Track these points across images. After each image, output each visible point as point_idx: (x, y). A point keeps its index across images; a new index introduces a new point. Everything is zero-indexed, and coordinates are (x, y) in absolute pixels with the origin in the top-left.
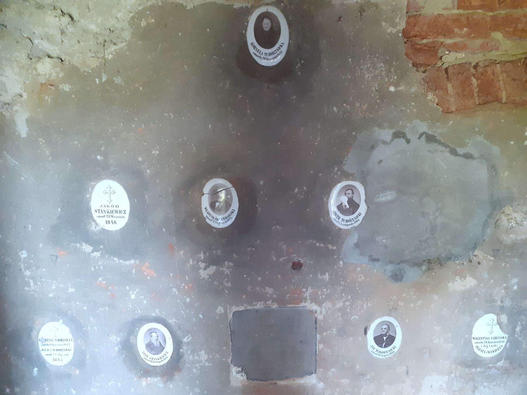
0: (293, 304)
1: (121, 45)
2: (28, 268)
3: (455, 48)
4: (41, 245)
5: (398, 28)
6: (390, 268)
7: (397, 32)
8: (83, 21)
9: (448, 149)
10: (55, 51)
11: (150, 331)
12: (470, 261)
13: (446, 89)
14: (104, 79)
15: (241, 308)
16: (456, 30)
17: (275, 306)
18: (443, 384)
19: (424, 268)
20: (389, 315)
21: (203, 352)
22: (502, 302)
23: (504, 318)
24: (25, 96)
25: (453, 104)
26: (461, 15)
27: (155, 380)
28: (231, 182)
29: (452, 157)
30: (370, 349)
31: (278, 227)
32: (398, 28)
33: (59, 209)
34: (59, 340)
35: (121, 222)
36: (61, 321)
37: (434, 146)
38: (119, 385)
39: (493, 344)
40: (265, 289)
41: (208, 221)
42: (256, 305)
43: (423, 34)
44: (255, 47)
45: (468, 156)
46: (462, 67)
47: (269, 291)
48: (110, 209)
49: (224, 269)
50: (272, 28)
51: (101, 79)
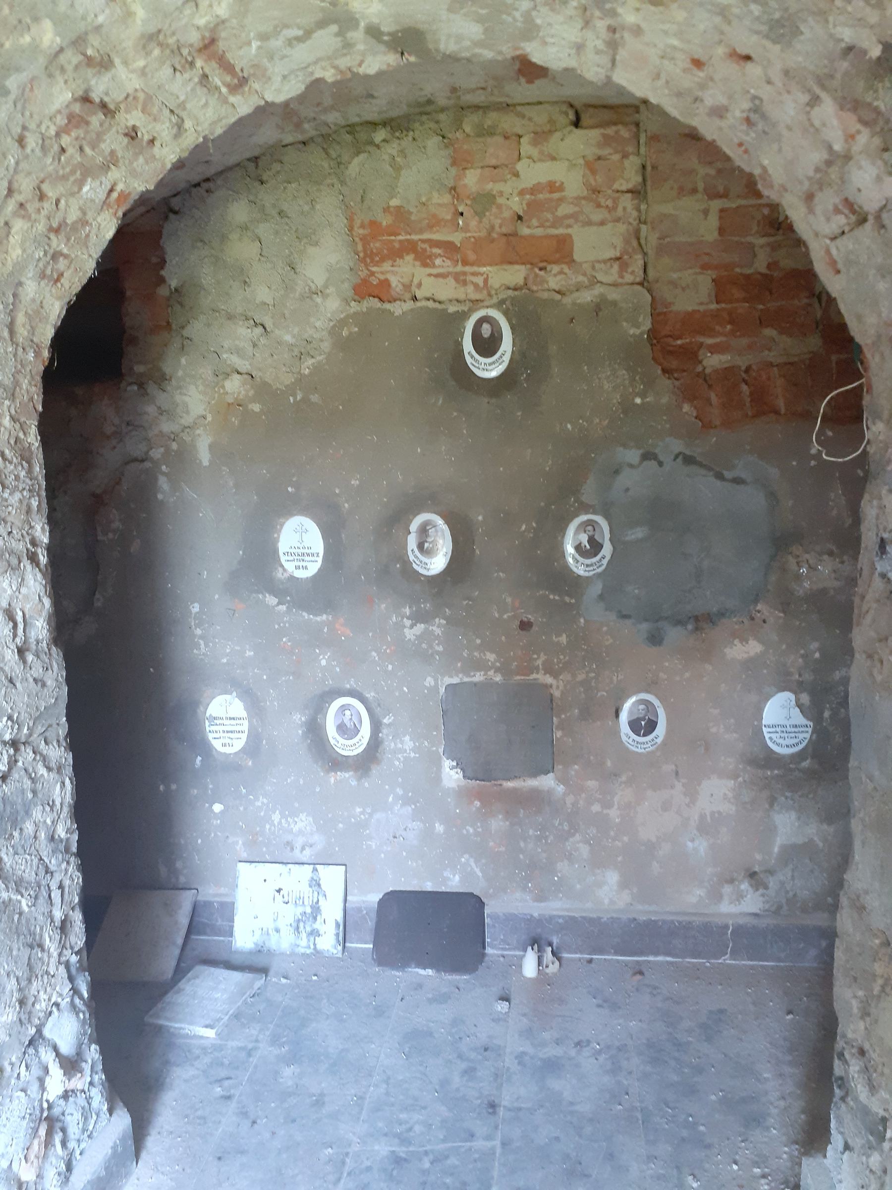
3: (714, 349)
4: (217, 597)
6: (645, 626)
7: (642, 334)
8: (277, 332)
10: (243, 365)
11: (344, 708)
12: (752, 619)
14: (299, 398)
15: (455, 680)
17: (498, 678)
18: (727, 792)
19: (690, 627)
21: (407, 738)
22: (800, 675)
23: (805, 698)
24: (209, 418)
26: (723, 309)
27: (347, 775)
29: (718, 483)
30: (624, 738)
31: (501, 574)
33: (241, 552)
34: (230, 719)
35: (313, 568)
36: (234, 694)
37: (694, 469)
40: (485, 655)
41: (414, 566)
42: (474, 676)
44: (472, 357)
45: (738, 481)
46: (729, 372)
48: (301, 551)
49: (434, 628)
50: (492, 334)
51: (295, 398)
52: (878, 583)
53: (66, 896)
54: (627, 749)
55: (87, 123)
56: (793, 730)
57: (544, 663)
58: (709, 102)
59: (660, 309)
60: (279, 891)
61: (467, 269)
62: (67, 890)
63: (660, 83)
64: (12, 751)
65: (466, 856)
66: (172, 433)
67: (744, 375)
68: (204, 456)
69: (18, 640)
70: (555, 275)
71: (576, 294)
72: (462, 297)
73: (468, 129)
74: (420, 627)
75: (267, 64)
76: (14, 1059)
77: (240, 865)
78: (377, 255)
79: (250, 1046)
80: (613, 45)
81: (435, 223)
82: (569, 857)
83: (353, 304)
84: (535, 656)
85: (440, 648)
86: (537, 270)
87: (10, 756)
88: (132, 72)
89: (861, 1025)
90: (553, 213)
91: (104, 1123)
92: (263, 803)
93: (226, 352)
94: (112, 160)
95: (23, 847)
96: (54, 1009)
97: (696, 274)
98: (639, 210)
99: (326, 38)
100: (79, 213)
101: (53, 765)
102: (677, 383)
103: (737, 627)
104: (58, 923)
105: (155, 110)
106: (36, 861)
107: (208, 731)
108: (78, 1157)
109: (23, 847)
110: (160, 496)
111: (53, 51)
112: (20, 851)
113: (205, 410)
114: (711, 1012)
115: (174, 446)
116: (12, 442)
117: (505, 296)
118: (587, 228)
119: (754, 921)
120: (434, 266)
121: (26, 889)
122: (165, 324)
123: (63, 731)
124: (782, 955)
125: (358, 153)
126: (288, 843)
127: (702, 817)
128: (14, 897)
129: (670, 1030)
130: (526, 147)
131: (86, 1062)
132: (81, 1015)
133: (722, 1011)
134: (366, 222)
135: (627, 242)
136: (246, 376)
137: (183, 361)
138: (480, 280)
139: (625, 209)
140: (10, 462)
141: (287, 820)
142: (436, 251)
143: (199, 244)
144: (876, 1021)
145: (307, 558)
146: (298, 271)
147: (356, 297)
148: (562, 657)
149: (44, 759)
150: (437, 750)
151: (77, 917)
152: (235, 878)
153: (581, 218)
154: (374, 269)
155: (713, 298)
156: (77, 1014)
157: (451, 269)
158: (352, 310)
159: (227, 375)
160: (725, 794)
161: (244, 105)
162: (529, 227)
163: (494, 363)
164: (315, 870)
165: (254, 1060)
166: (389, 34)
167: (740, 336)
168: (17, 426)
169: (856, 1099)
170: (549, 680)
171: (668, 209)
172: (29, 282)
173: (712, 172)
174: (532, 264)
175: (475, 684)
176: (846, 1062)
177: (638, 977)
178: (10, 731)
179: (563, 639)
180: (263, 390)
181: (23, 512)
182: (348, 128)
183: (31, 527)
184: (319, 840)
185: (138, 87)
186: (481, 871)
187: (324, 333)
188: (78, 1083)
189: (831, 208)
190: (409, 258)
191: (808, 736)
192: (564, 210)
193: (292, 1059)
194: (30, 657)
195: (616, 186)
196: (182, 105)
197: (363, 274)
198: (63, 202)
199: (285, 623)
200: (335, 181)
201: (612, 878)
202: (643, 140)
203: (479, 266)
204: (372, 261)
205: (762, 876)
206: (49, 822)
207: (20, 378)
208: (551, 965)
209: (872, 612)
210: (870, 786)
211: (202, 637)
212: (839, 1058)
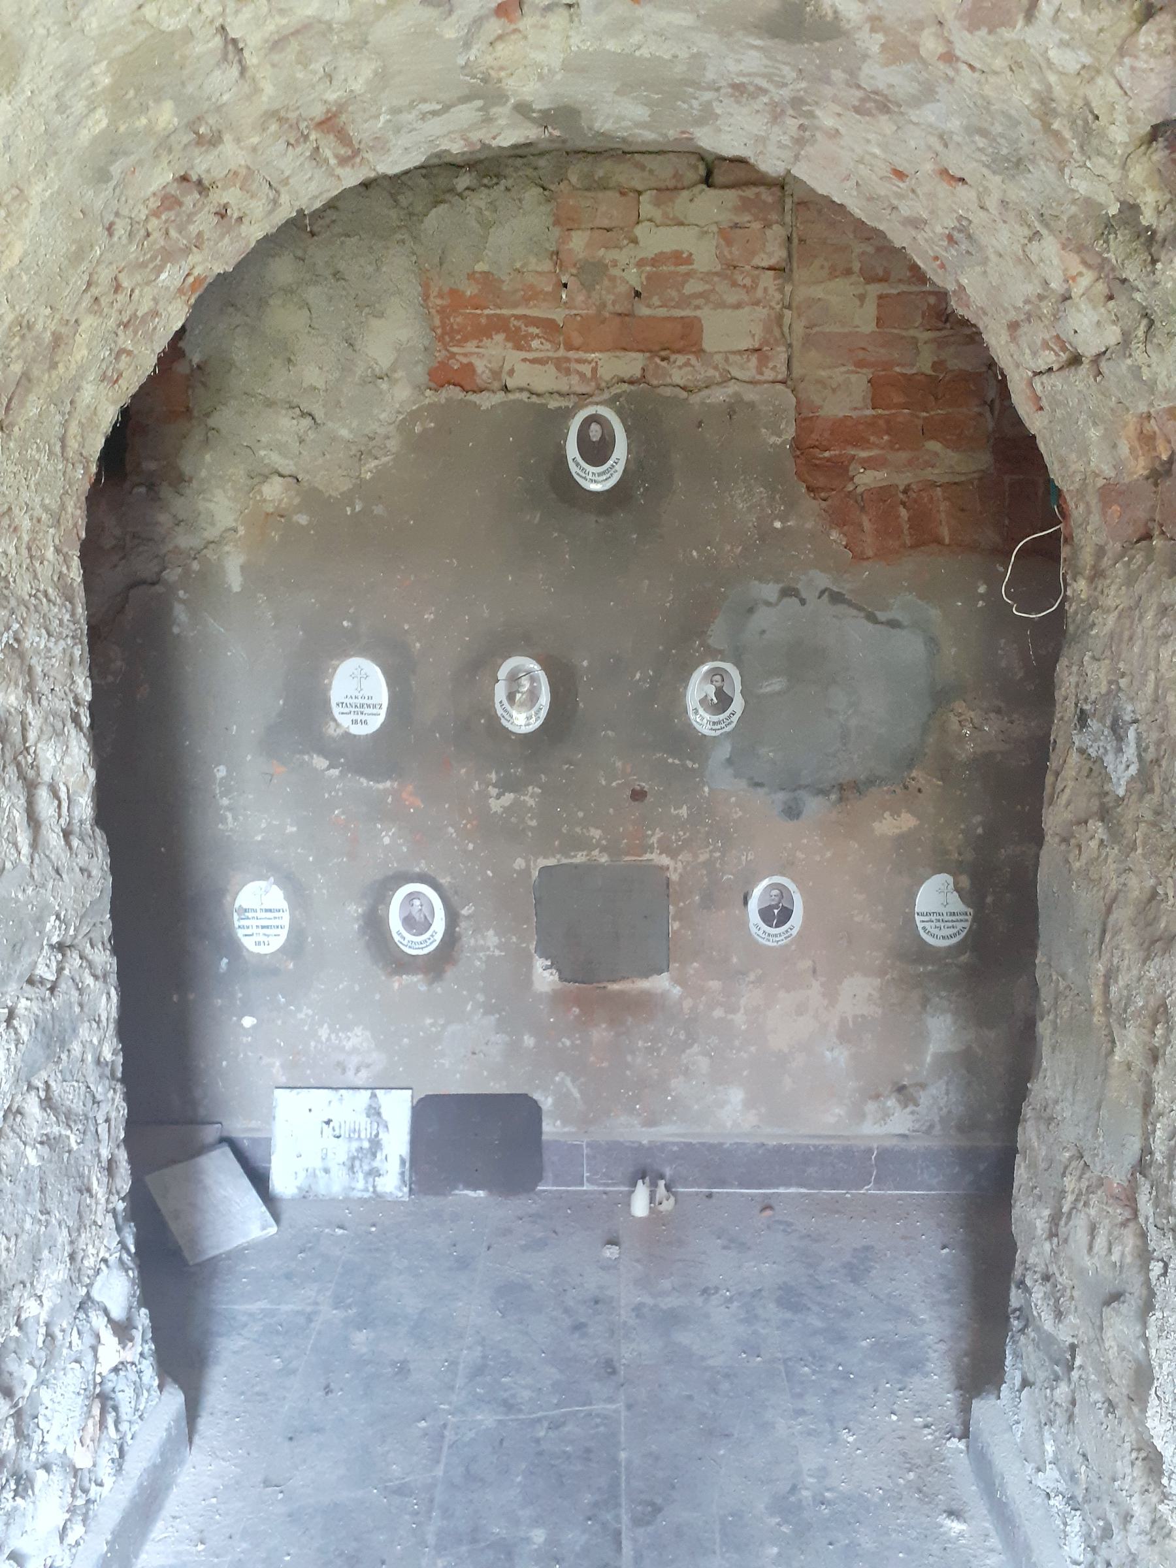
0: (633, 855)
1: (384, 459)
2: (224, 794)
3: (868, 464)
4: (249, 757)
5: (784, 437)
6: (781, 796)
7: (784, 443)
8: (330, 424)
9: (862, 614)
10: (286, 465)
11: (411, 896)
12: (906, 788)
13: (860, 525)
14: (358, 508)
15: (551, 862)
16: (872, 439)
17: (604, 859)
18: (873, 993)
19: (833, 797)
20: (783, 875)
21: (491, 933)
22: (960, 854)
23: (965, 881)
24: (242, 531)
25: (869, 543)
26: (879, 416)
27: (415, 979)
28: (539, 662)
29: (870, 626)
30: (753, 930)
31: (610, 733)
32: (784, 437)
33: (281, 702)
34: (266, 911)
35: (376, 721)
36: (272, 879)
37: (842, 608)
38: (357, 988)
39: (950, 924)
40: (588, 831)
41: (503, 721)
42: (575, 856)
43: (825, 443)
44: (578, 464)
45: (893, 624)
46: (883, 494)
47: (596, 833)
48: (361, 701)
49: (527, 798)
50: (603, 437)
51: (353, 509)
52: (1074, 758)
53: (112, 1131)
54: (757, 942)
55: (180, 204)
56: (951, 918)
57: (660, 840)
58: (905, 211)
59: (806, 413)
60: (328, 1122)
61: (572, 354)
62: (113, 1123)
63: (851, 183)
64: (60, 957)
65: (561, 1074)
66: (191, 548)
67: (901, 496)
68: (235, 580)
69: (62, 821)
70: (680, 368)
71: (705, 392)
72: (565, 389)
73: (574, 179)
74: (509, 798)
75: (391, 137)
76: (65, 1325)
77: (278, 1092)
78: (458, 332)
79: (309, 1309)
80: (800, 142)
81: (531, 295)
82: (686, 1072)
83: (428, 393)
84: (649, 832)
85: (534, 823)
86: (658, 360)
87: (59, 963)
88: (242, 149)
89: (1047, 1246)
90: (678, 291)
91: (154, 1403)
92: (306, 1015)
93: (264, 448)
94: (198, 242)
95: (71, 1072)
96: (103, 1266)
97: (848, 372)
98: (781, 290)
99: (466, 114)
100: (152, 303)
101: (99, 972)
102: (824, 504)
103: (887, 797)
104: (105, 1164)
105: (254, 187)
106: (83, 1088)
107: (236, 925)
108: (130, 1442)
109: (71, 1072)
110: (176, 630)
111: (166, 133)
112: (68, 1077)
113: (236, 520)
114: (855, 1250)
115: (195, 566)
116: (56, 579)
117: (619, 391)
118: (719, 310)
119: (903, 1144)
120: (530, 350)
121: (75, 1121)
122: (183, 409)
123: (106, 931)
124: (934, 1182)
125: (437, 203)
126: (339, 1064)
127: (843, 1021)
128: (63, 1132)
129: (811, 1272)
130: (647, 207)
131: (136, 1328)
132: (130, 1273)
133: (867, 1248)
134: (446, 289)
135: (768, 330)
136: (290, 479)
137: (208, 457)
138: (586, 369)
139: (766, 289)
140: (54, 604)
141: (337, 1035)
142: (534, 330)
143: (231, 309)
144: (1066, 1241)
145: (366, 710)
146: (357, 348)
147: (432, 385)
148: (681, 833)
149: (91, 965)
150: (528, 946)
151: (122, 1155)
152: (271, 1108)
153: (713, 298)
154: (455, 349)
155: (869, 401)
156: (127, 1272)
157: (551, 354)
158: (427, 401)
159: (266, 478)
160: (870, 995)
161: (351, 178)
162: (649, 306)
163: (604, 473)
164: (374, 1096)
165: (316, 1325)
166: (540, 111)
167: (898, 450)
168: (61, 558)
169: (1038, 1329)
170: (665, 860)
171: (818, 292)
172: (88, 386)
173: (870, 250)
174: (650, 351)
175: (576, 866)
176: (1027, 1290)
177: (768, 1213)
178: (57, 932)
179: (684, 812)
180: (312, 498)
181: (67, 664)
182: (424, 171)
183: (73, 682)
184: (378, 1059)
185: (243, 163)
186: (581, 1092)
187: (392, 428)
188: (130, 1354)
189: (1039, 342)
190: (500, 337)
191: (967, 925)
192: (692, 287)
193: (363, 1322)
194: (75, 843)
195: (756, 261)
196: (285, 182)
197: (441, 355)
198: (137, 292)
199: (337, 791)
200: (406, 236)
201: (736, 1096)
202: (788, 207)
203: (586, 352)
204: (452, 339)
205: (911, 1090)
206: (95, 1041)
207: (66, 498)
208: (665, 1202)
209: (1068, 791)
210: (1062, 985)
211: (229, 808)
212: (1018, 1287)
